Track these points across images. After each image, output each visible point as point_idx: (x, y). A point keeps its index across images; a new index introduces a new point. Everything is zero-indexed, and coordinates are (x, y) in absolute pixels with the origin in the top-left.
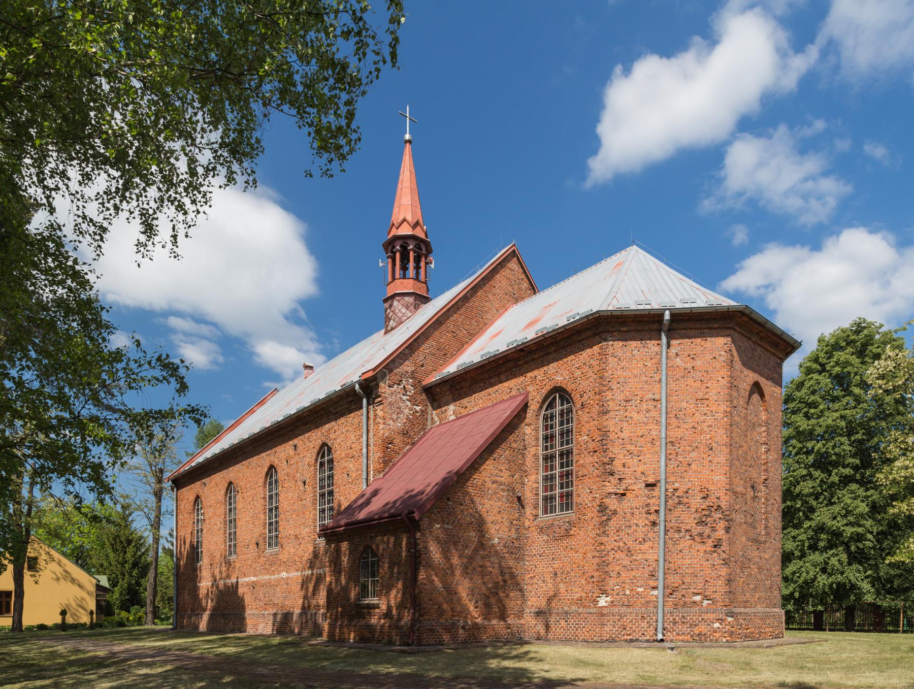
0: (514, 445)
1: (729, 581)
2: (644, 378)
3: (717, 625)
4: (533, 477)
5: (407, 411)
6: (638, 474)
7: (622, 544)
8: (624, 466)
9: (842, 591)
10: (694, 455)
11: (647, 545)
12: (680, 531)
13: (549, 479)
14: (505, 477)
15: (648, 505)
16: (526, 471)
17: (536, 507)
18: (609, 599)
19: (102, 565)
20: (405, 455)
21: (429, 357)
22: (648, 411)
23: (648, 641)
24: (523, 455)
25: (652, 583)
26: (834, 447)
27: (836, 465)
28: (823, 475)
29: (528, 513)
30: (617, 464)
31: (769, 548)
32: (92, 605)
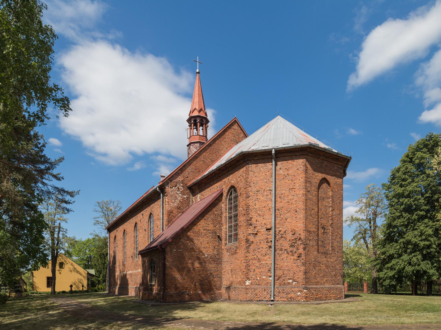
0: (216, 213)
1: (305, 273)
2: (265, 181)
3: (299, 293)
4: (224, 227)
5: (179, 198)
6: (263, 225)
7: (255, 257)
8: (256, 221)
9: (419, 275)
10: (288, 214)
11: (267, 257)
12: (282, 250)
13: (230, 227)
14: (211, 227)
15: (267, 238)
16: (222, 224)
17: (226, 240)
18: (250, 282)
19: (95, 265)
20: (179, 217)
21: (191, 173)
22: (267, 195)
23: (267, 301)
24: (221, 217)
25: (269, 274)
26: (414, 201)
27: (416, 210)
28: (409, 216)
29: (223, 243)
30: (253, 220)
31: (334, 256)
32: (85, 283)
